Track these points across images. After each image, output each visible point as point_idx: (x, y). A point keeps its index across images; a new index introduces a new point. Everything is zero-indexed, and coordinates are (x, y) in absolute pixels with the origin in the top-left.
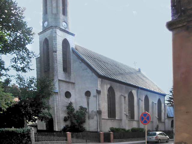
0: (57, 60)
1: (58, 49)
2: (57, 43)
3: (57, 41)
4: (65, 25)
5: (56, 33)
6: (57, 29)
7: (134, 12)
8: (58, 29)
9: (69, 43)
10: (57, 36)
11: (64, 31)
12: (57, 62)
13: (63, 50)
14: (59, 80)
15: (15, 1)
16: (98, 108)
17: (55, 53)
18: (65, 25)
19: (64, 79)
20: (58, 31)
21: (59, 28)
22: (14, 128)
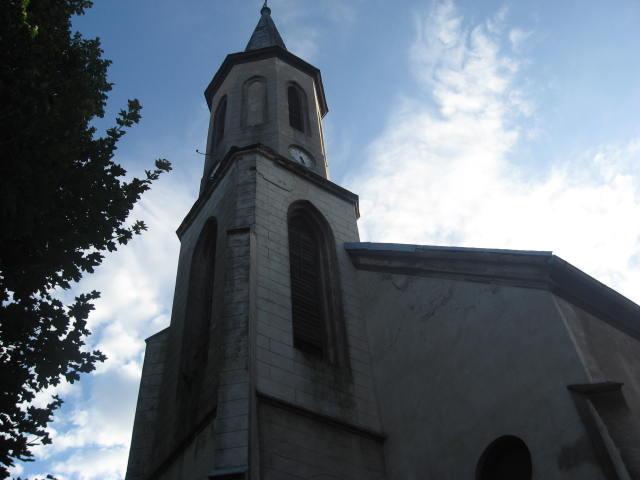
0: (248, 268)
1: (260, 218)
2: (258, 204)
3: (259, 196)
4: (301, 158)
5: (254, 168)
6: (258, 157)
7: (37, 28)
8: (263, 155)
9: (325, 223)
10: (259, 179)
11: (298, 170)
12: (247, 280)
13: (293, 257)
14: (263, 400)
15: (266, 10)
16: (215, 171)
17: (243, 237)
18: (301, 158)
19: (303, 400)
20: (266, 169)
21: (271, 151)
22: (101, 114)
